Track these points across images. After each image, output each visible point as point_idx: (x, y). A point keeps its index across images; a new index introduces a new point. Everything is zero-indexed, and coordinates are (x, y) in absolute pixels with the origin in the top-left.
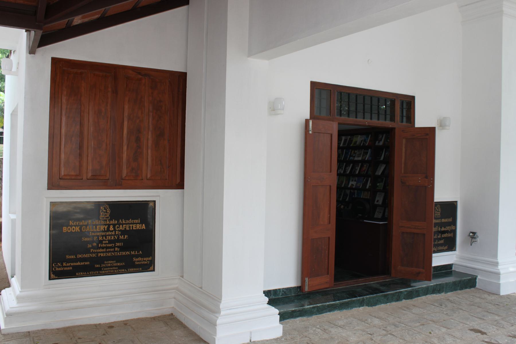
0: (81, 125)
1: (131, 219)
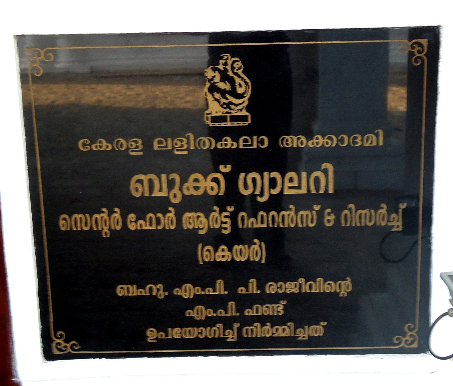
0: (124, 291)
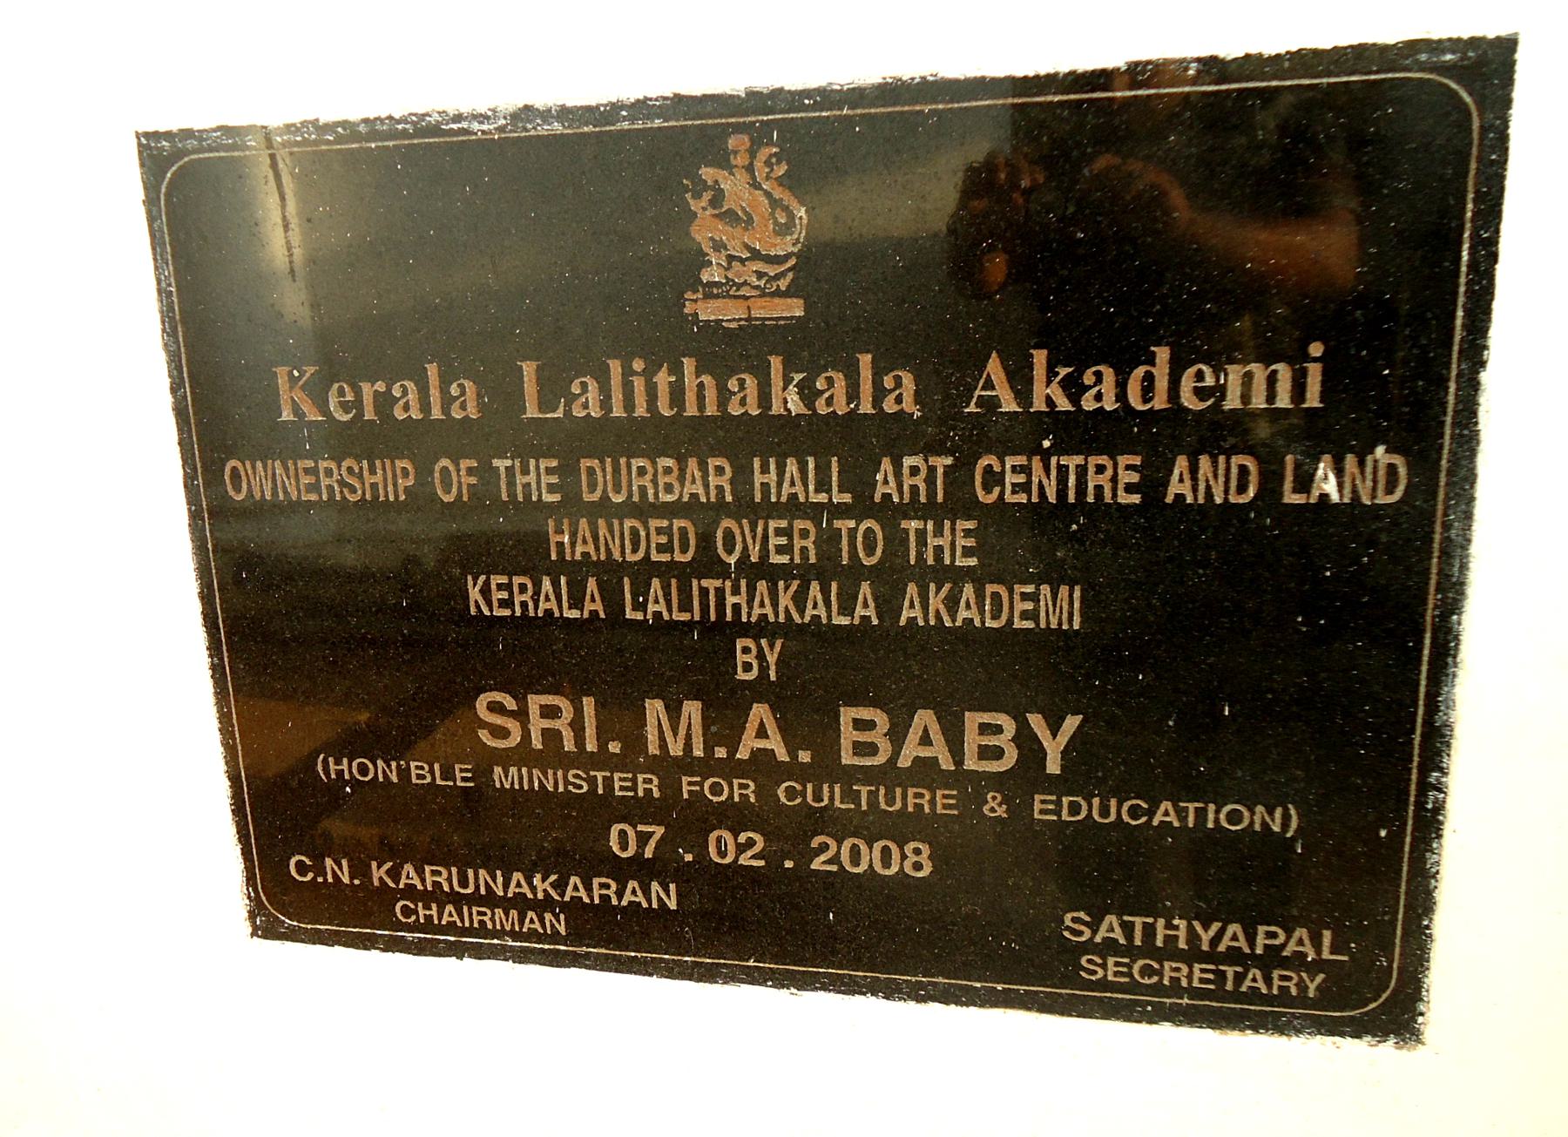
1: (1163, 354)
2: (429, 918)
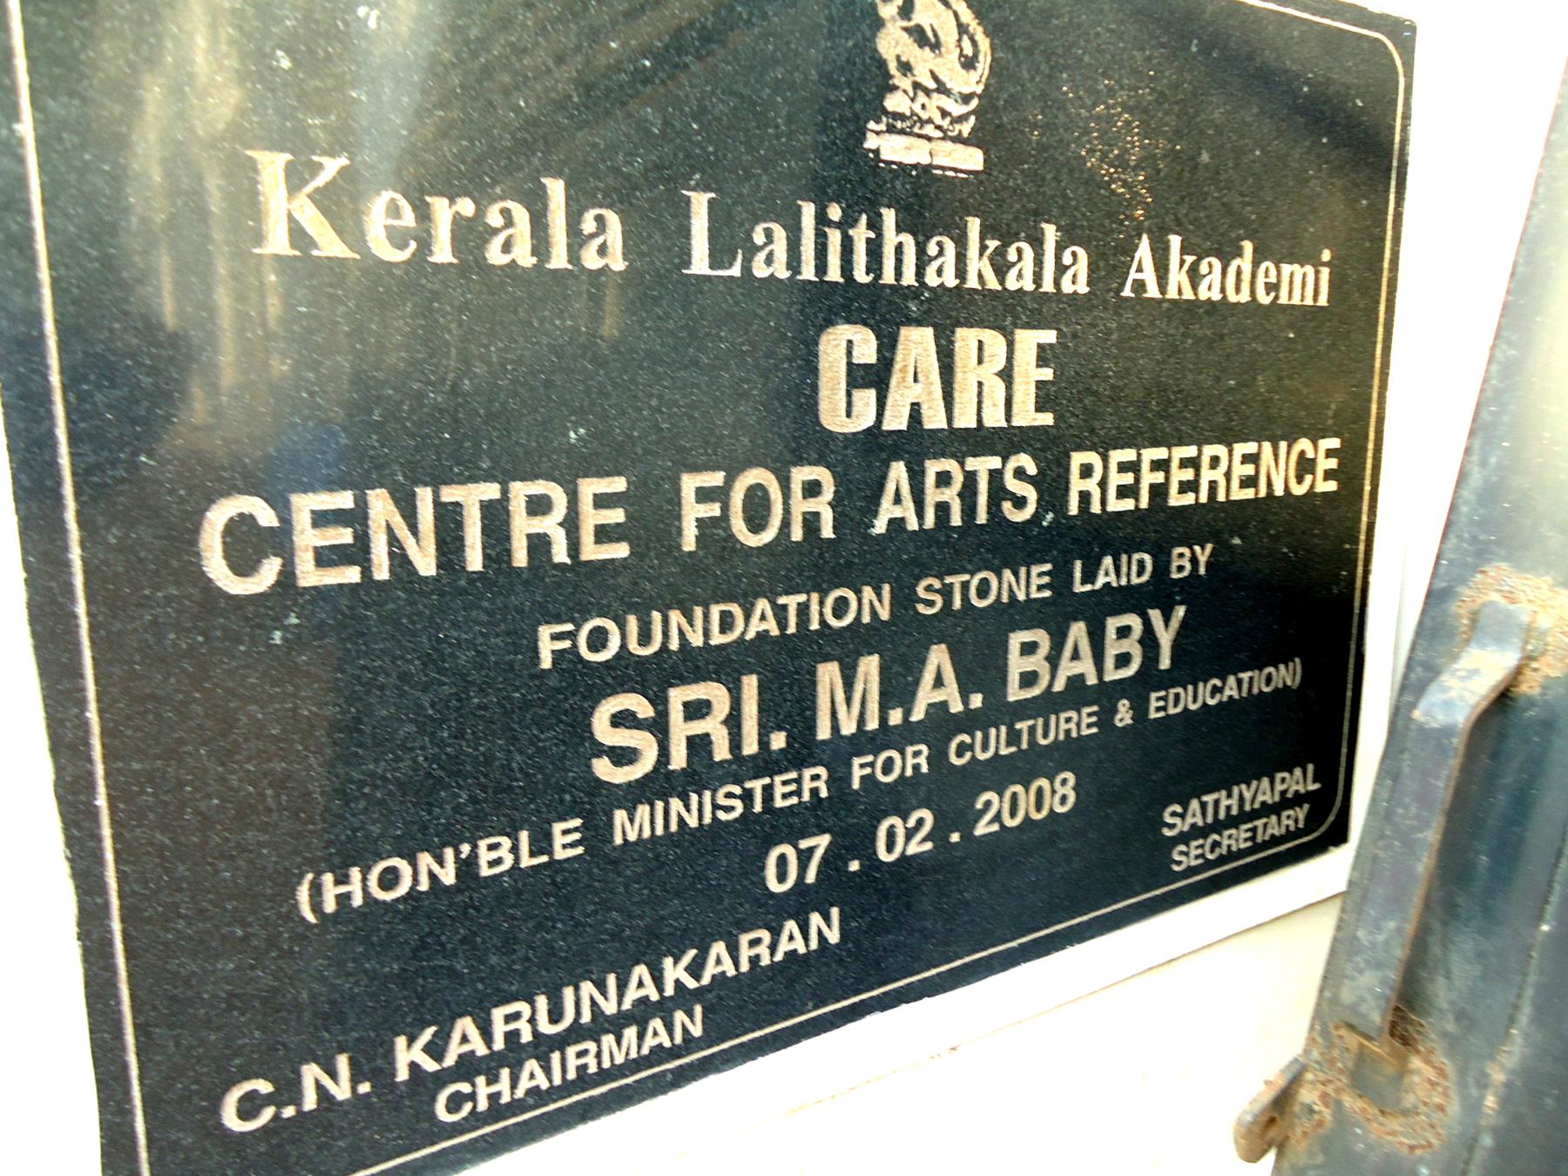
2: (494, 1098)
